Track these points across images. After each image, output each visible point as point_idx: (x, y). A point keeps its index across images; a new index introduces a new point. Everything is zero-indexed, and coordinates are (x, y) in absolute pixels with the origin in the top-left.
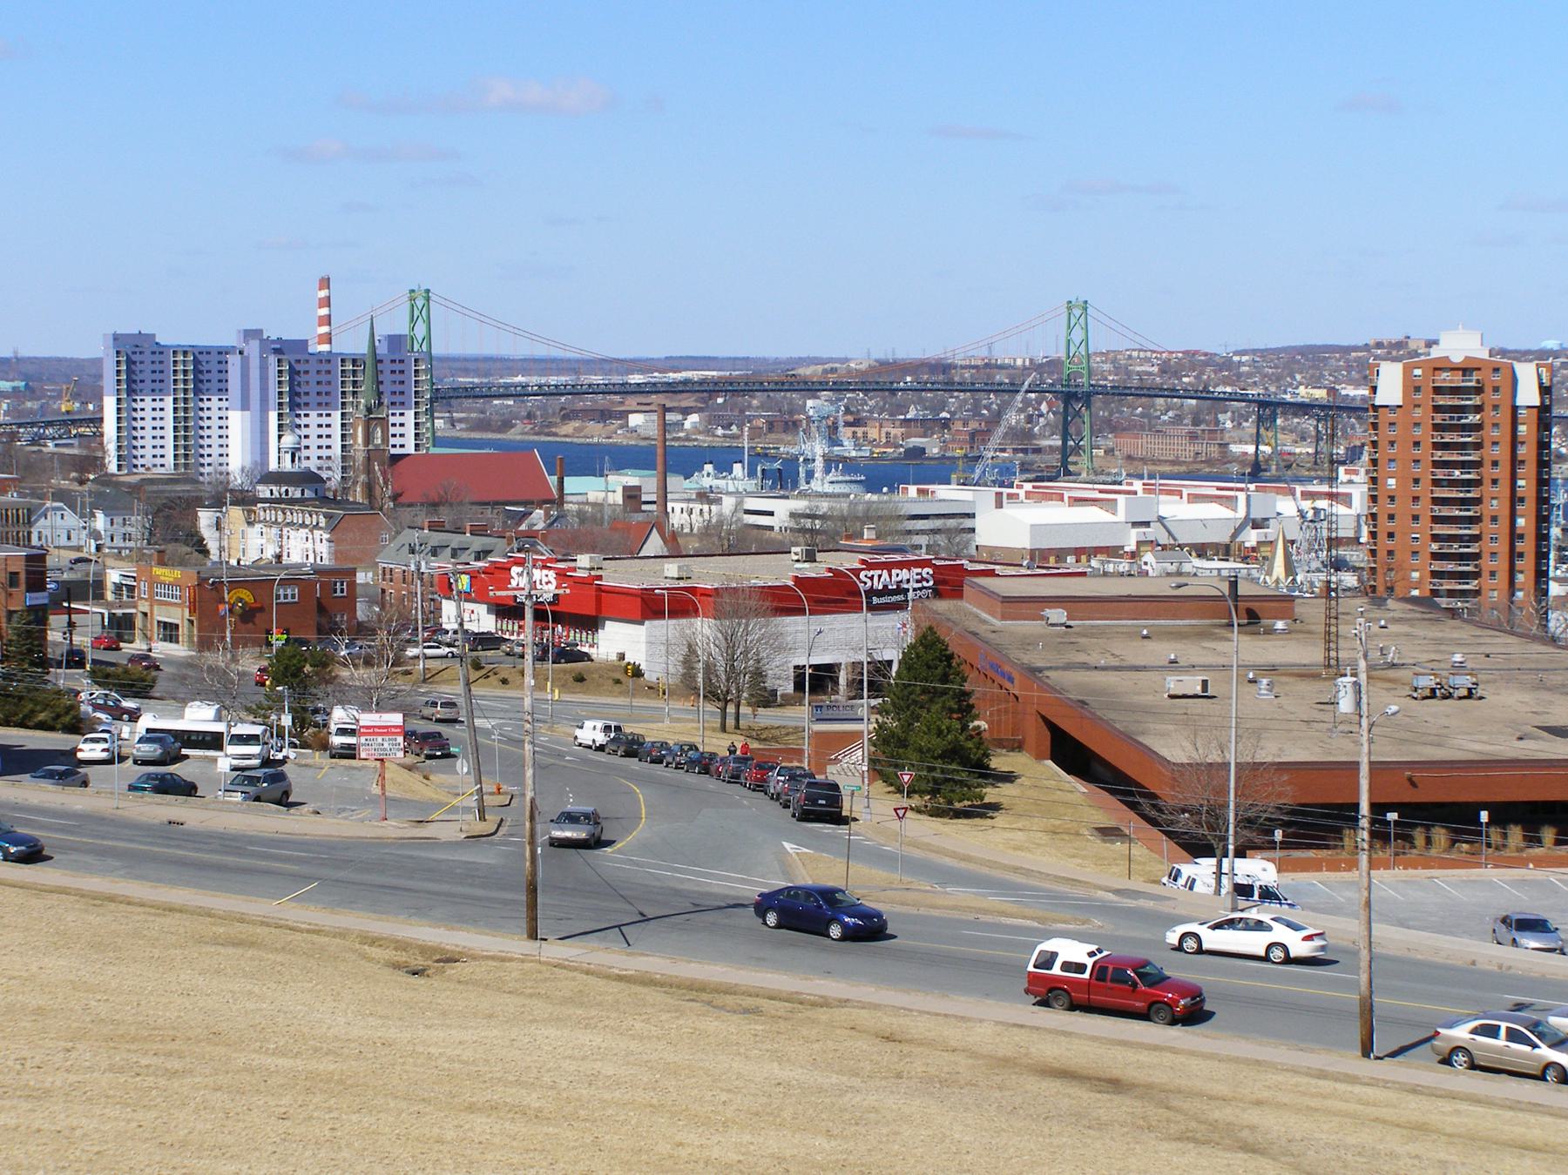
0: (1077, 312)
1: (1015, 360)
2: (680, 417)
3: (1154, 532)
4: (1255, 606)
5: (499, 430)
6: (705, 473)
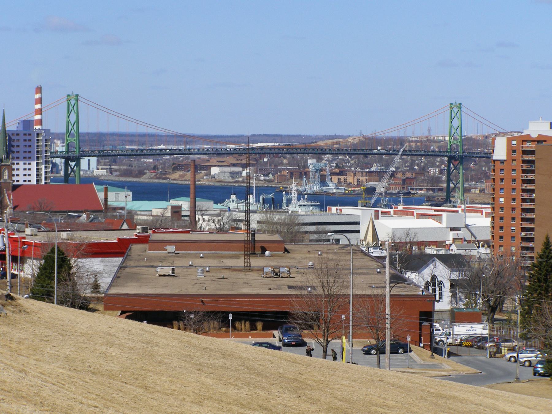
0: (456, 110)
1: (445, 138)
2: (240, 169)
3: (463, 233)
4: (265, 245)
5: (136, 176)
6: (231, 200)
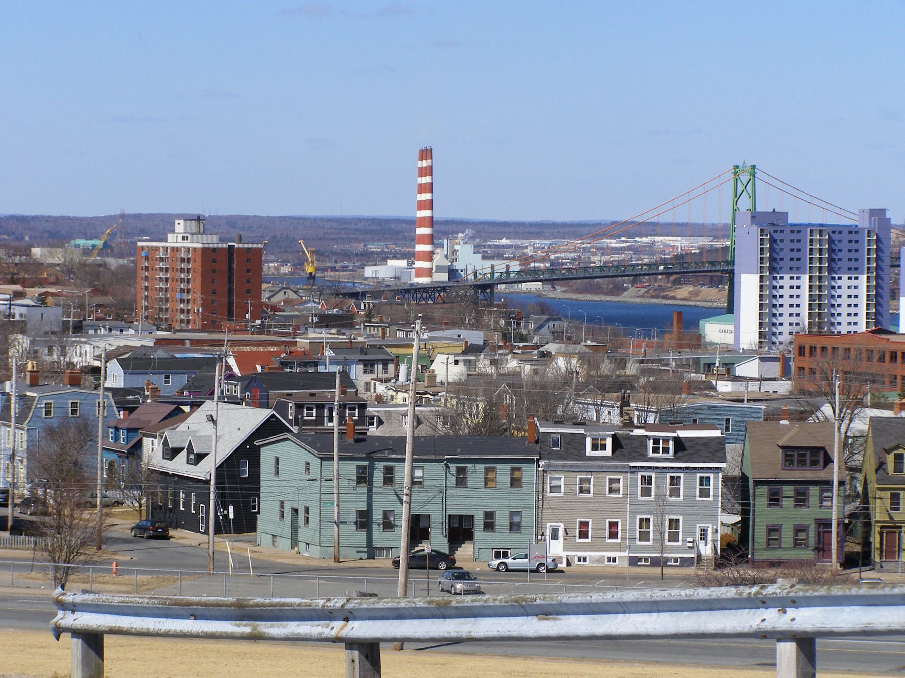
0: (745, 178)
